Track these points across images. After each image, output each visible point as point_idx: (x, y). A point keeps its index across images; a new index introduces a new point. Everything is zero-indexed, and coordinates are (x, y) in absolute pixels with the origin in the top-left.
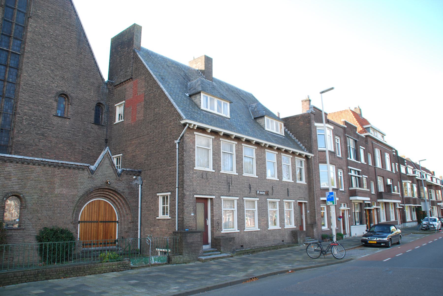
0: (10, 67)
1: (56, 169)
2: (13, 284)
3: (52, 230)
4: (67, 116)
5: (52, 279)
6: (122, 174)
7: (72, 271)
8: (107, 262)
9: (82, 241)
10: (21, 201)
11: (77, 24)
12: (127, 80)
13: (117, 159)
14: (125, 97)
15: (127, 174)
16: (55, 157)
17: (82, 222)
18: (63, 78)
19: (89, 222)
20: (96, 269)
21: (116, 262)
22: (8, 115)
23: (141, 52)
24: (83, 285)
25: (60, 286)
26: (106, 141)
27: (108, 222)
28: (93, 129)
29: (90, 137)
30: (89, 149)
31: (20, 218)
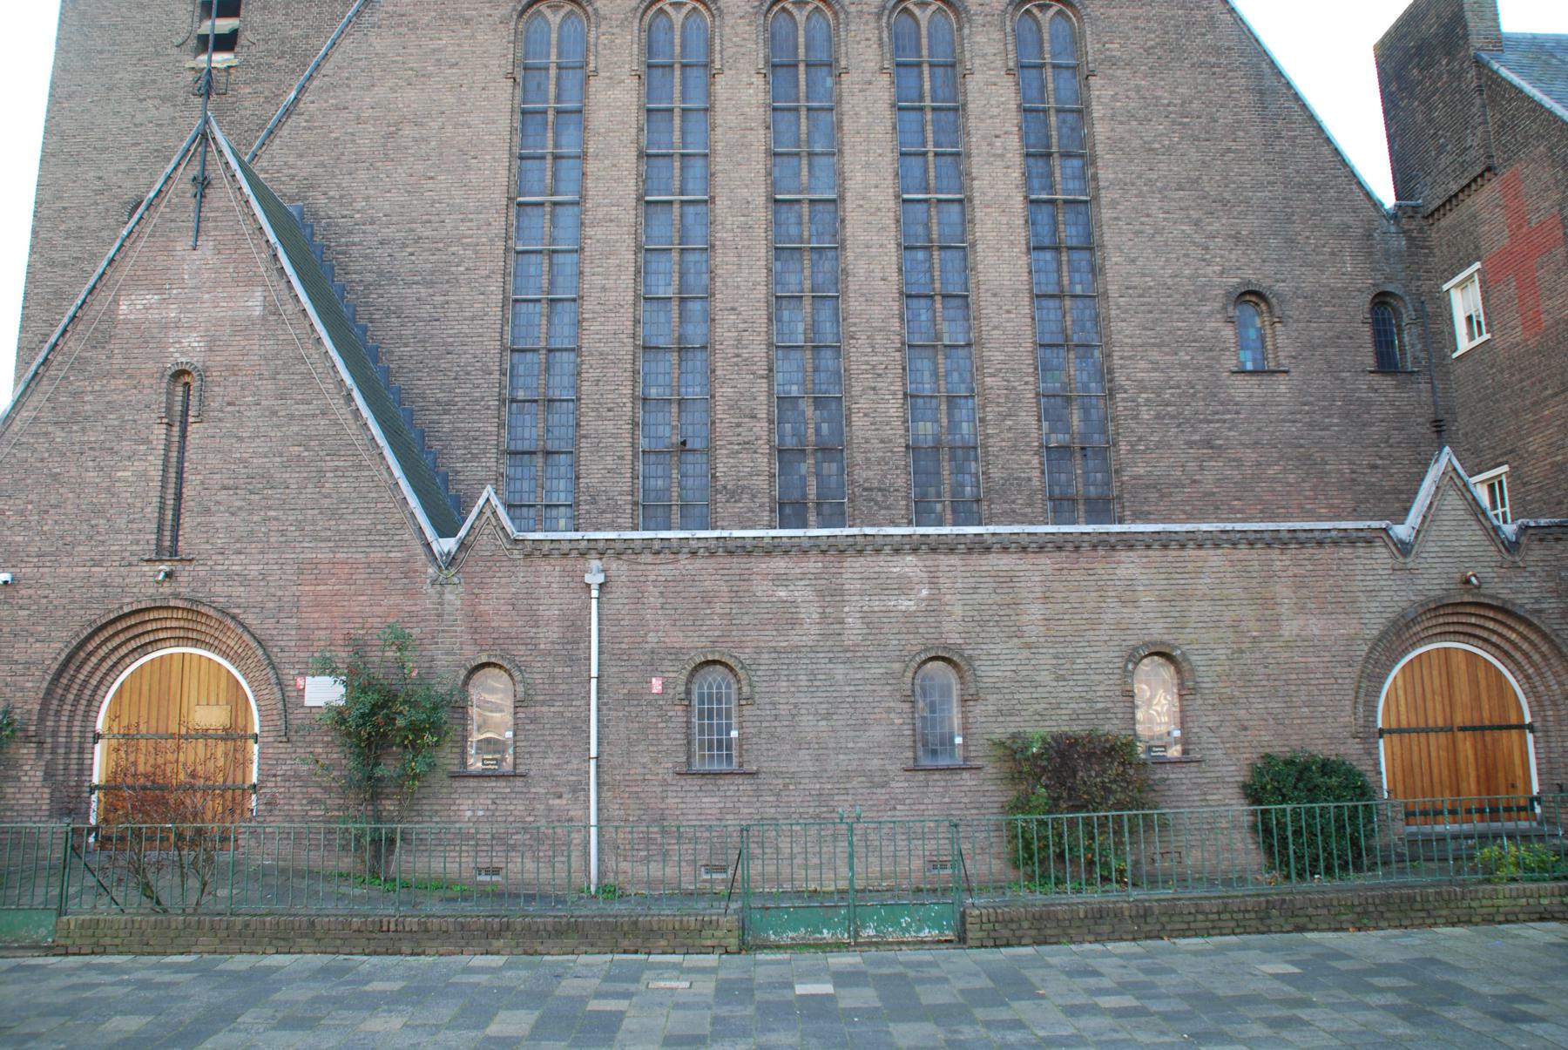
0: (1070, 248)
1: (1275, 554)
2: (1196, 935)
3: (1290, 763)
4: (1278, 365)
5: (1316, 930)
6: (1523, 540)
7: (1382, 908)
8: (1514, 880)
9: (1400, 800)
10: (1179, 671)
11: (1240, 41)
12: (1475, 180)
13: (1491, 488)
14: (1477, 248)
15: (1541, 540)
16: (1262, 511)
17: (1390, 732)
18: (1237, 238)
19: (1417, 731)
20: (1474, 904)
21: (1553, 884)
22: (1094, 401)
23: (1509, 56)
24: (1433, 961)
25: (1349, 957)
26: (1438, 426)
27: (1492, 728)
28: (1376, 391)
29: (1372, 424)
30: (1375, 467)
31: (1183, 725)
